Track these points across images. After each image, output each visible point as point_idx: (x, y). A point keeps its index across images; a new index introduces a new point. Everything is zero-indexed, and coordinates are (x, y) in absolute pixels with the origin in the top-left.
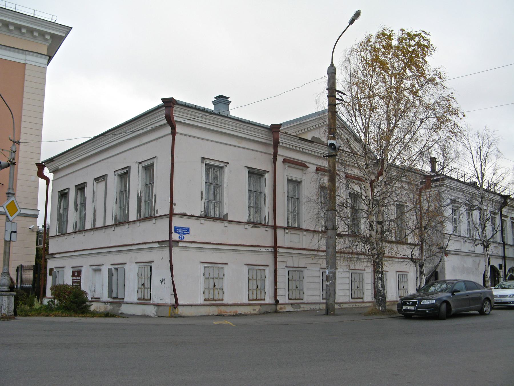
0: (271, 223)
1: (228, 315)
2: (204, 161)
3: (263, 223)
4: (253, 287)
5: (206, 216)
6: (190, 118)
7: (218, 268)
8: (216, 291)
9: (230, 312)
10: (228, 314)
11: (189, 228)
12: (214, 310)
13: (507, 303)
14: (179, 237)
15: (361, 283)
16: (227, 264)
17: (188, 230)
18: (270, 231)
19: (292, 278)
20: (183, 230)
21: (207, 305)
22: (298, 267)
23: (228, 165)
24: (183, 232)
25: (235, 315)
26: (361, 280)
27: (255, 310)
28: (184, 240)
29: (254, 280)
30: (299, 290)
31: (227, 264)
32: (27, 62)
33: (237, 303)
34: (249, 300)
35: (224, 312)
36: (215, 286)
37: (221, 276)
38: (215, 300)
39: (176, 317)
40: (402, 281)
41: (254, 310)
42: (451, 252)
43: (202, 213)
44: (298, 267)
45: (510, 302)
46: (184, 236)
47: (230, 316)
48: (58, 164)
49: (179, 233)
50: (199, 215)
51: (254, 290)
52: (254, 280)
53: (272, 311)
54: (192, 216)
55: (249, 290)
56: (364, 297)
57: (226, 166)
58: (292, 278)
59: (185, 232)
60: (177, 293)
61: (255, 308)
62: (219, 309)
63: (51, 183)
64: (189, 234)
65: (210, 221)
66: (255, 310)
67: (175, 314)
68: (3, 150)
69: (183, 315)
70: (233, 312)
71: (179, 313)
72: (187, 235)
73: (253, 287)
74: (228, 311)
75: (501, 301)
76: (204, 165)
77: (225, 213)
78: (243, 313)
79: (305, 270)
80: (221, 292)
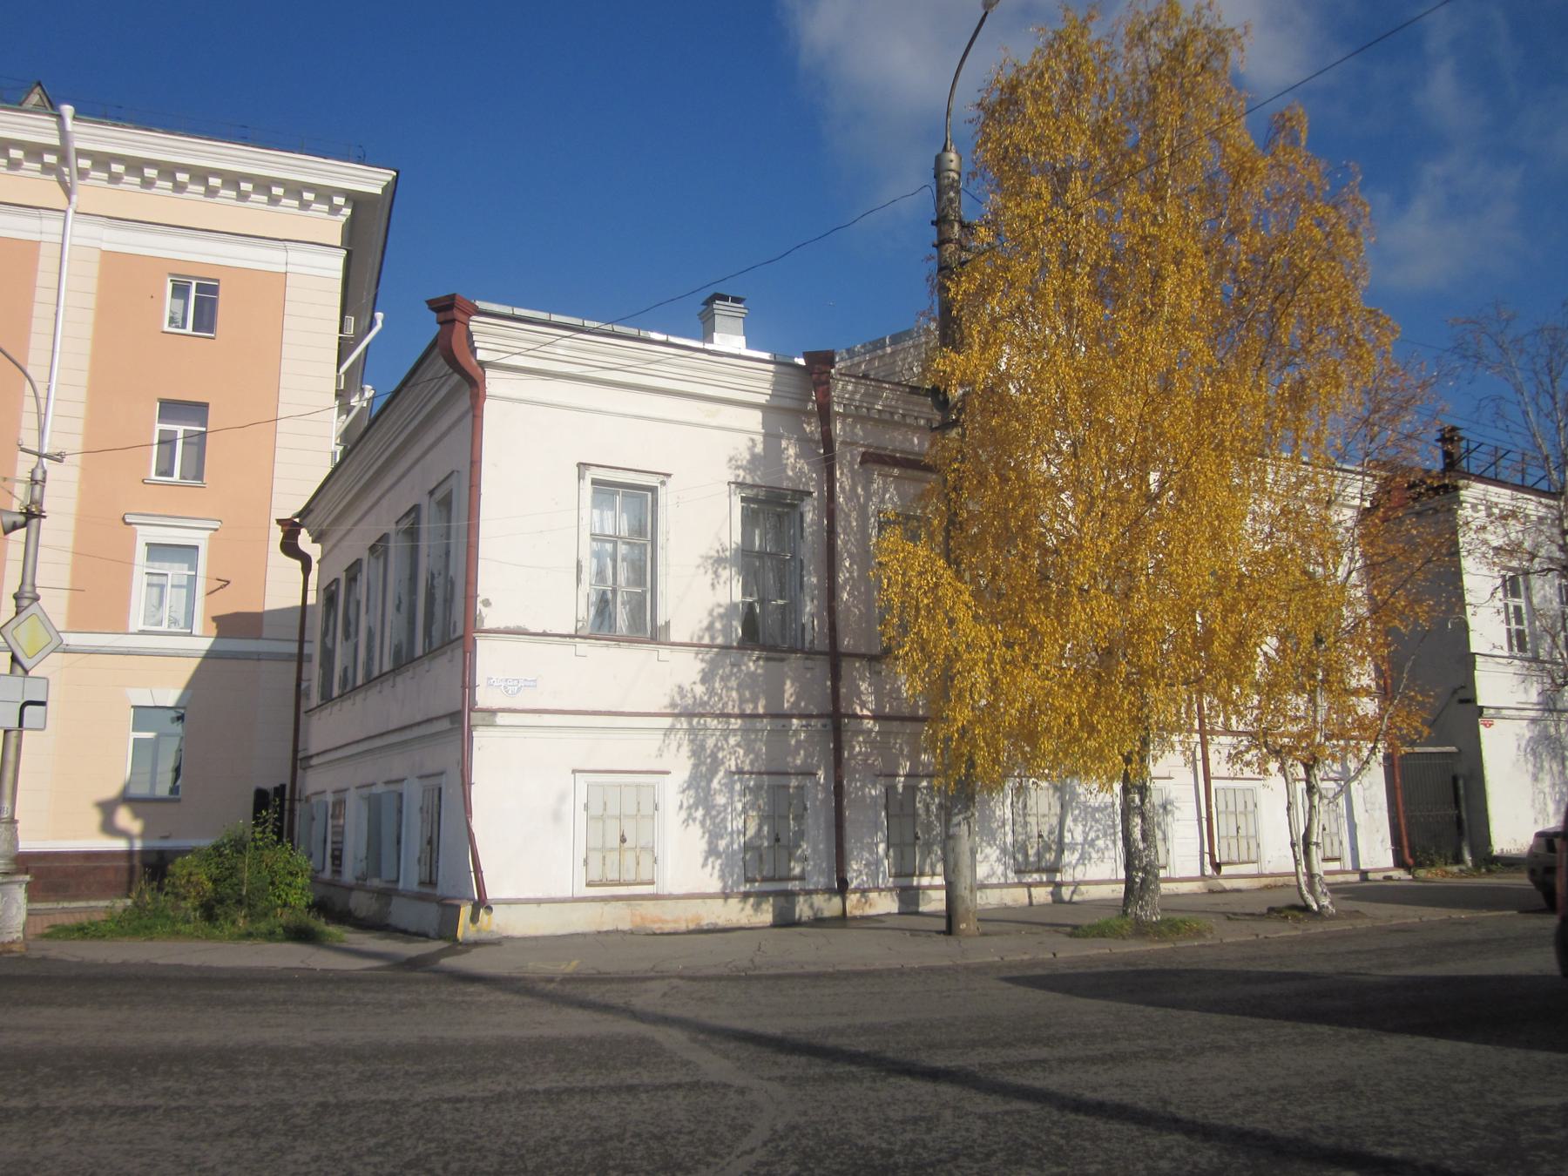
0: (822, 644)
1: (666, 930)
3: (799, 646)
6: (517, 351)
8: (629, 858)
9: (675, 921)
15: (1250, 817)
16: (668, 773)
18: (821, 666)
19: (902, 809)
21: (594, 899)
23: (670, 482)
26: (1250, 807)
29: (1231, 813)
31: (668, 773)
32: (290, 268)
34: (589, 884)
35: (654, 922)
36: (623, 840)
37: (647, 809)
40: (1231, 808)
42: (1504, 712)
43: (580, 624)
48: (319, 518)
54: (544, 634)
56: (1171, 863)
57: (663, 483)
58: (902, 809)
60: (483, 868)
63: (315, 566)
65: (607, 646)
68: (5, 479)
70: (686, 920)
80: (646, 860)
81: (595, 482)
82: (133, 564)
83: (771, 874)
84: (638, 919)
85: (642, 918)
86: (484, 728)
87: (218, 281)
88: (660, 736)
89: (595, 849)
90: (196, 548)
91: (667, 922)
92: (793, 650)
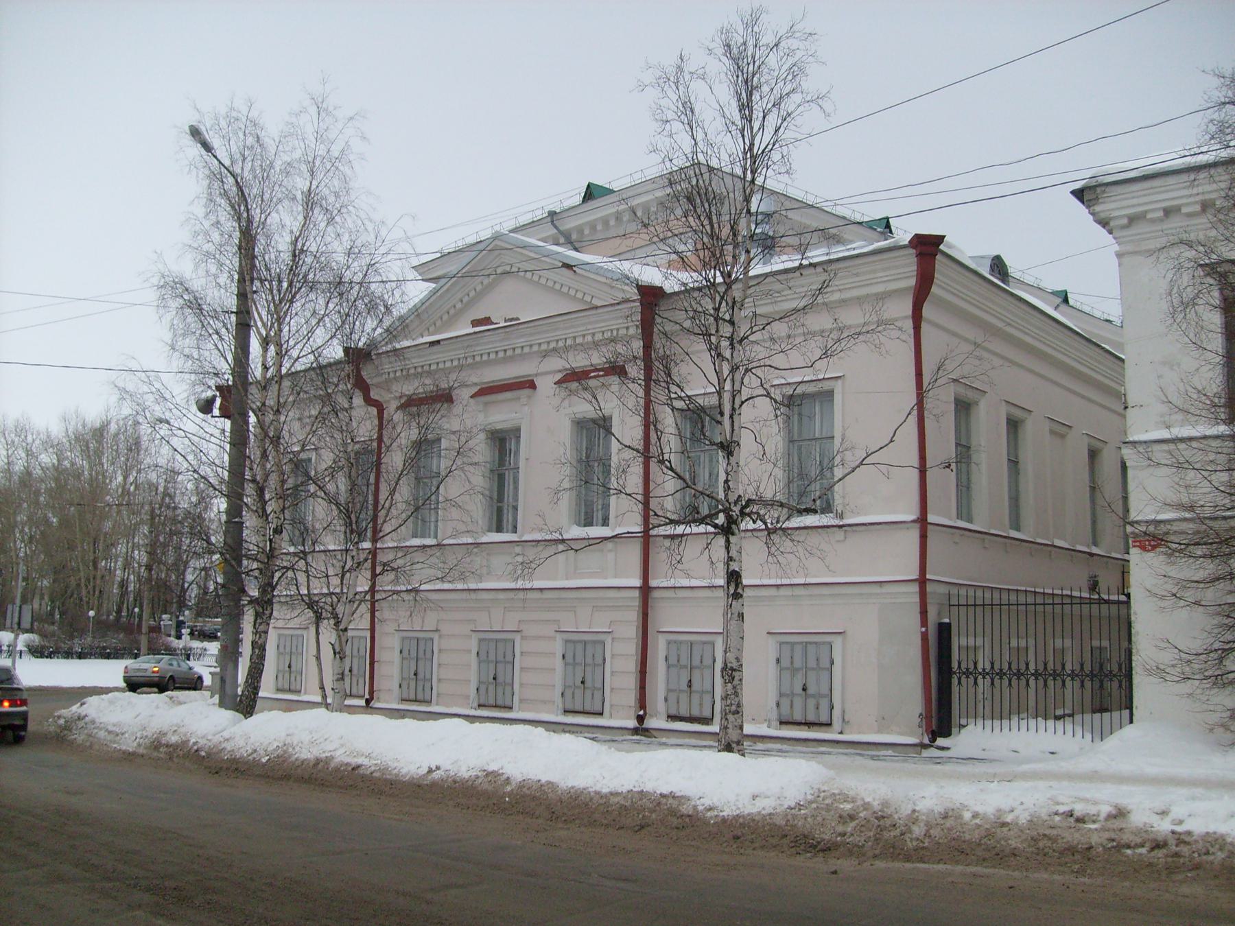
8: (811, 703)
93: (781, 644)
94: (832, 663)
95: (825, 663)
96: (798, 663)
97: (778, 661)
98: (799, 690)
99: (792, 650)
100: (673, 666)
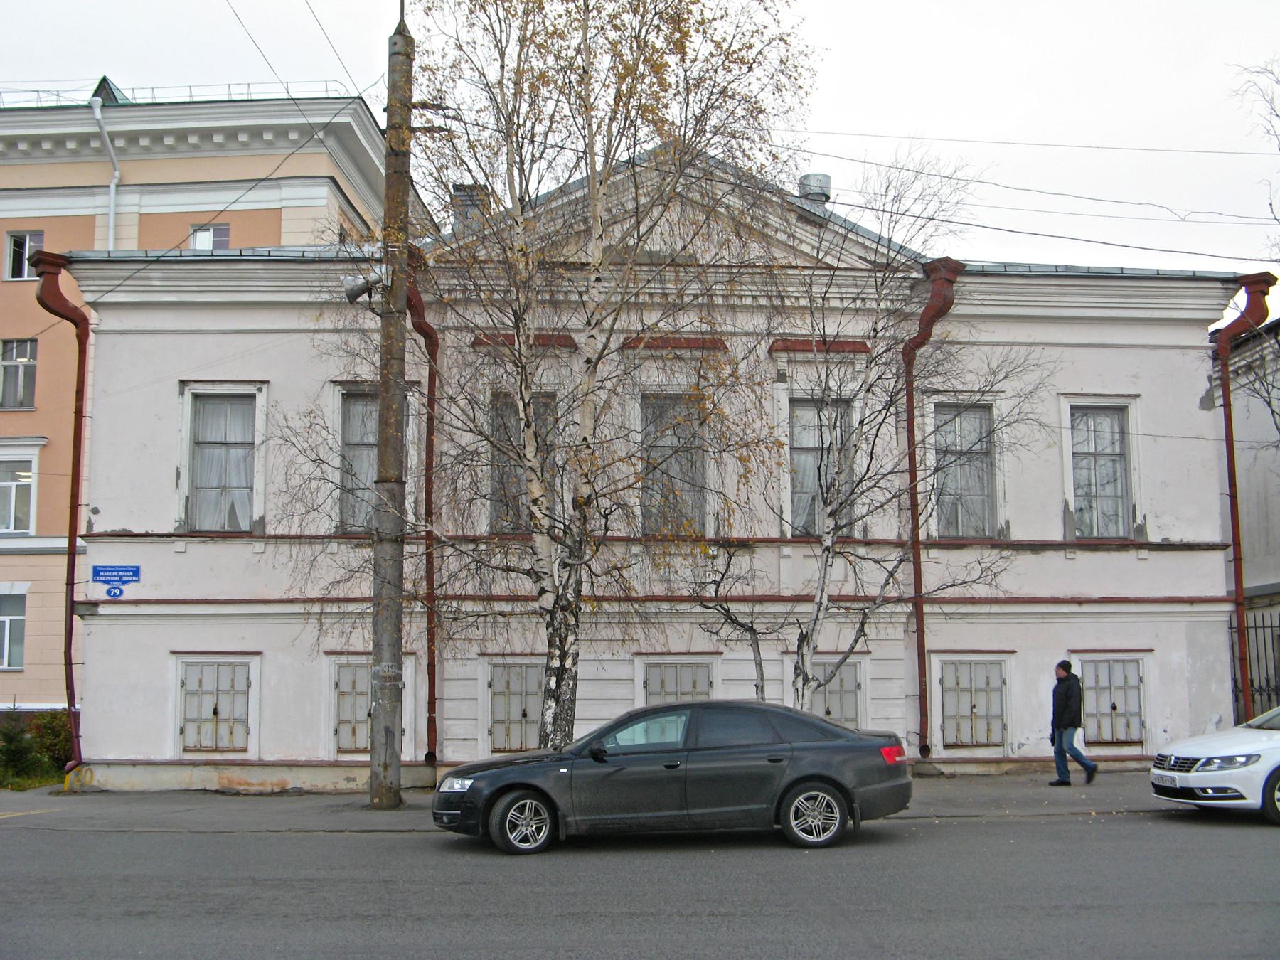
1: (253, 792)
2: (187, 389)
4: (354, 713)
5: (189, 532)
6: (110, 288)
7: (230, 664)
8: (1121, 722)
9: (261, 784)
10: (253, 789)
11: (138, 568)
12: (210, 778)
13: (1187, 793)
14: (109, 592)
17: (136, 571)
20: (121, 574)
22: (532, 654)
24: (121, 577)
25: (280, 792)
27: (354, 780)
28: (122, 598)
29: (963, 690)
30: (1123, 715)
31: (1013, 652)
33: (294, 758)
35: (240, 784)
36: (1114, 708)
38: (223, 751)
39: (84, 793)
41: (349, 780)
44: (532, 654)
45: (1204, 790)
46: (123, 587)
47: (260, 794)
49: (107, 582)
50: (170, 530)
51: (962, 717)
52: (963, 690)
53: (419, 784)
54: (147, 535)
55: (494, 722)
59: (124, 579)
61: (352, 775)
62: (225, 775)
64: (138, 581)
66: (354, 780)
67: (82, 785)
69: (109, 787)
70: (272, 784)
71: (95, 783)
72: (132, 584)
73: (354, 713)
74: (254, 781)
75: (1169, 785)
76: (188, 397)
77: (1001, 522)
78: (306, 787)
79: (716, 662)
80: (239, 729)
81: (196, 396)
82: (40, 474)
83: (518, 747)
84: (225, 782)
85: (229, 780)
86: (91, 618)
87: (228, 224)
88: (313, 622)
89: (951, 717)
90: (30, 462)
91: (252, 785)
92: (678, 538)
93: (340, 666)
94: (249, 685)
95: (240, 686)
96: (1104, 682)
97: (183, 684)
98: (1107, 709)
99: (1096, 669)
100: (950, 690)
